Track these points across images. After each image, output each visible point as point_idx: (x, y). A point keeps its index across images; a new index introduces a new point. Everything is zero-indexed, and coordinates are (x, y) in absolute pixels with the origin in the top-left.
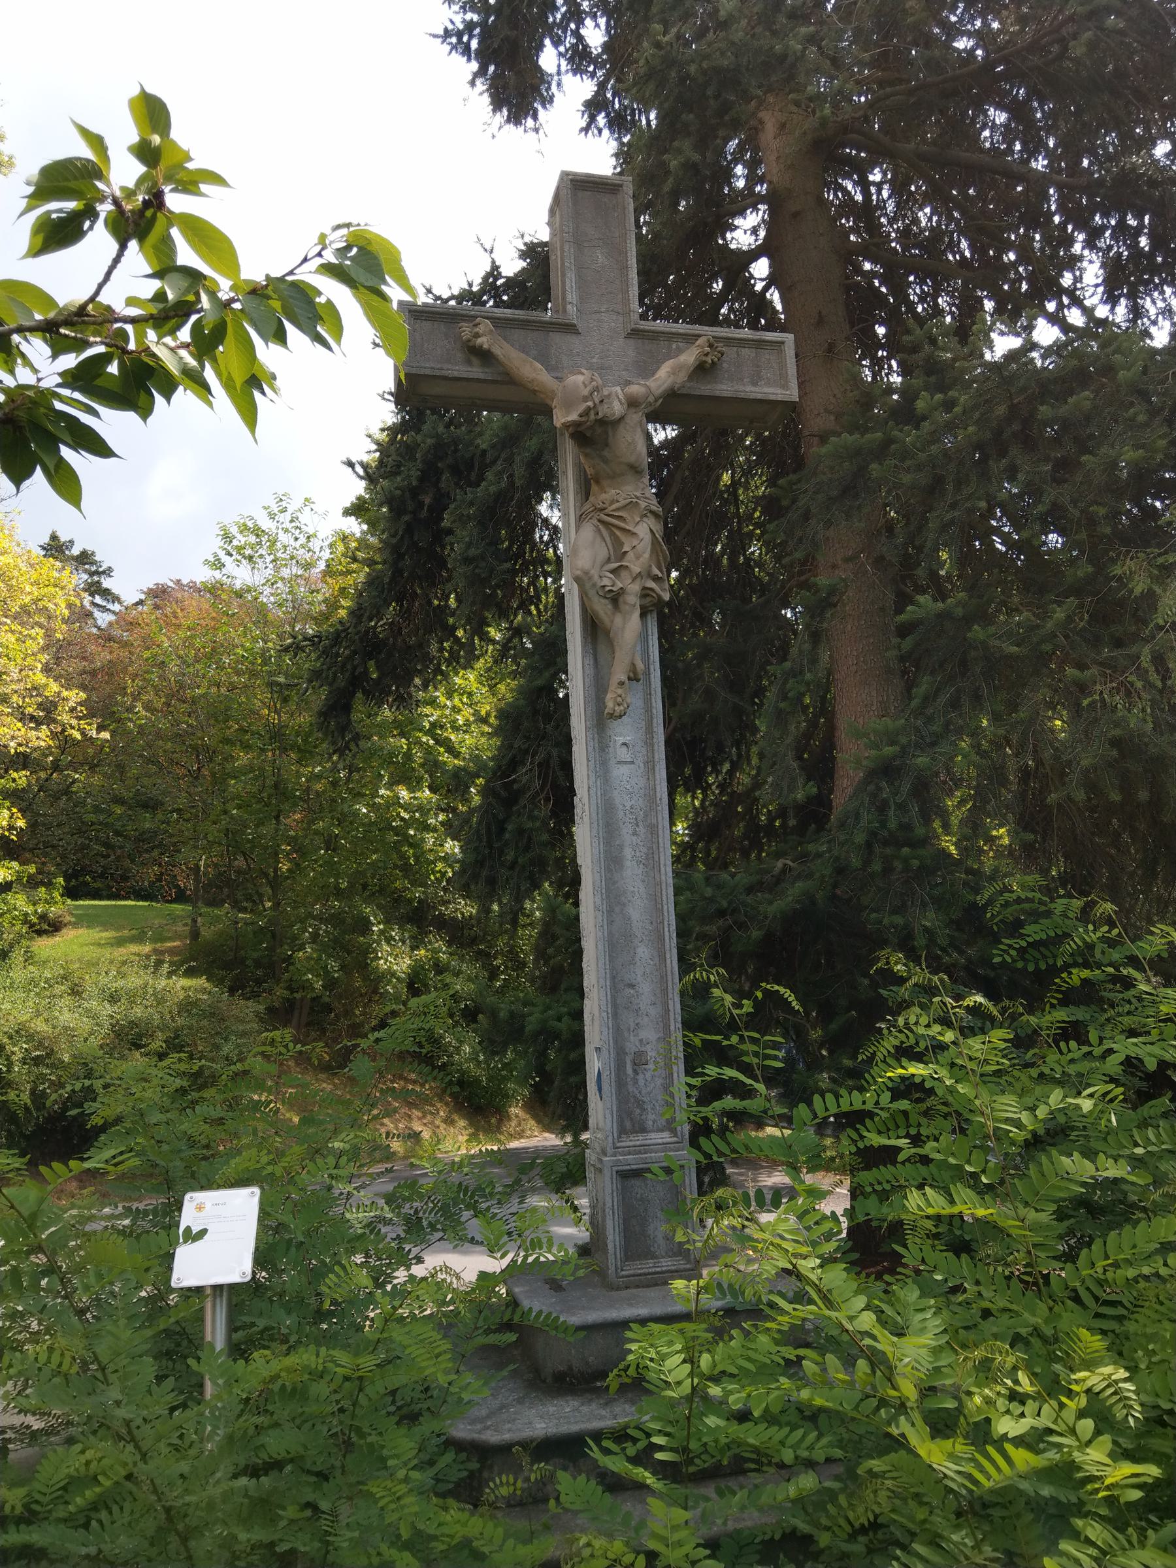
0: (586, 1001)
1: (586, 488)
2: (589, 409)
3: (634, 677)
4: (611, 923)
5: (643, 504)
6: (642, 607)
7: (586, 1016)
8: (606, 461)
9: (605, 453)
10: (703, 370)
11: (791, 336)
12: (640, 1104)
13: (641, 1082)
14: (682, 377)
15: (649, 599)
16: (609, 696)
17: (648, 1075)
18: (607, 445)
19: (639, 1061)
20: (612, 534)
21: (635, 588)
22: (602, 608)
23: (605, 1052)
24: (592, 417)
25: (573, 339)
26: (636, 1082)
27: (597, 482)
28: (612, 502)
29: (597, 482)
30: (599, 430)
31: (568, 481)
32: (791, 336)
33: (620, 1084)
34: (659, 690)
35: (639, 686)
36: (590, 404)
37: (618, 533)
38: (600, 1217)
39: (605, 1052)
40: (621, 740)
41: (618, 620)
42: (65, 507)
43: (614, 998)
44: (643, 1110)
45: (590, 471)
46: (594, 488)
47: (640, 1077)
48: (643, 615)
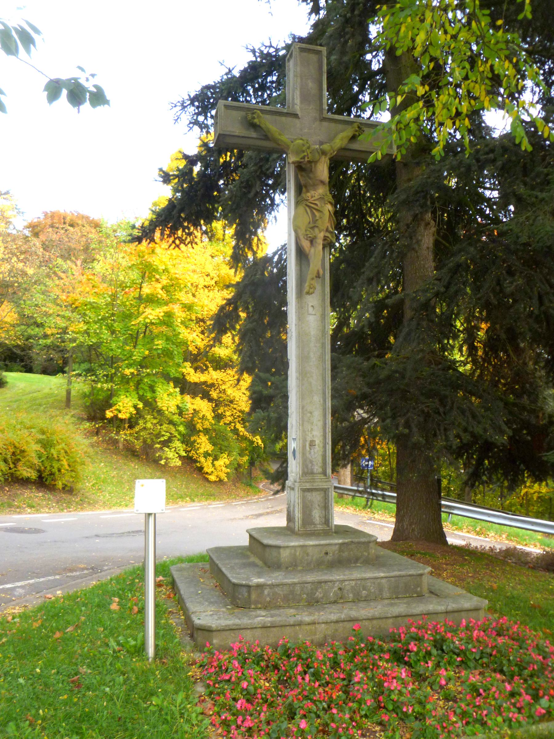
0: (289, 419)
1: (300, 189)
2: (305, 156)
3: (318, 276)
4: (303, 385)
5: (326, 199)
6: (323, 245)
7: (289, 425)
8: (310, 178)
9: (311, 175)
10: (353, 138)
11: (325, 48)
12: (311, 462)
13: (312, 453)
14: (346, 141)
15: (326, 242)
16: (307, 284)
17: (316, 450)
18: (311, 171)
19: (312, 444)
20: (311, 211)
21: (322, 235)
22: (306, 244)
23: (298, 440)
24: (306, 159)
25: (296, 121)
26: (310, 453)
27: (306, 187)
28: (312, 197)
29: (306, 187)
30: (308, 165)
31: (291, 185)
32: (325, 48)
33: (304, 454)
34: (329, 282)
35: (320, 280)
36: (305, 154)
37: (314, 211)
38: (292, 509)
39: (298, 440)
40: (310, 304)
41: (312, 250)
42: (27, 55)
43: (303, 417)
44: (313, 465)
45: (303, 182)
46: (304, 189)
47: (312, 451)
48: (323, 248)
